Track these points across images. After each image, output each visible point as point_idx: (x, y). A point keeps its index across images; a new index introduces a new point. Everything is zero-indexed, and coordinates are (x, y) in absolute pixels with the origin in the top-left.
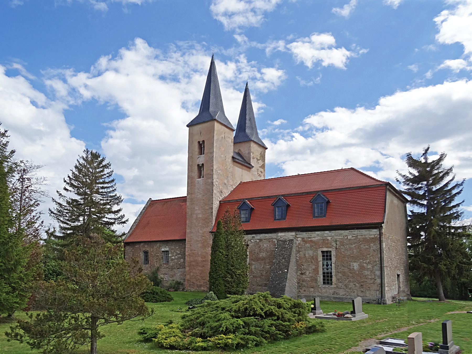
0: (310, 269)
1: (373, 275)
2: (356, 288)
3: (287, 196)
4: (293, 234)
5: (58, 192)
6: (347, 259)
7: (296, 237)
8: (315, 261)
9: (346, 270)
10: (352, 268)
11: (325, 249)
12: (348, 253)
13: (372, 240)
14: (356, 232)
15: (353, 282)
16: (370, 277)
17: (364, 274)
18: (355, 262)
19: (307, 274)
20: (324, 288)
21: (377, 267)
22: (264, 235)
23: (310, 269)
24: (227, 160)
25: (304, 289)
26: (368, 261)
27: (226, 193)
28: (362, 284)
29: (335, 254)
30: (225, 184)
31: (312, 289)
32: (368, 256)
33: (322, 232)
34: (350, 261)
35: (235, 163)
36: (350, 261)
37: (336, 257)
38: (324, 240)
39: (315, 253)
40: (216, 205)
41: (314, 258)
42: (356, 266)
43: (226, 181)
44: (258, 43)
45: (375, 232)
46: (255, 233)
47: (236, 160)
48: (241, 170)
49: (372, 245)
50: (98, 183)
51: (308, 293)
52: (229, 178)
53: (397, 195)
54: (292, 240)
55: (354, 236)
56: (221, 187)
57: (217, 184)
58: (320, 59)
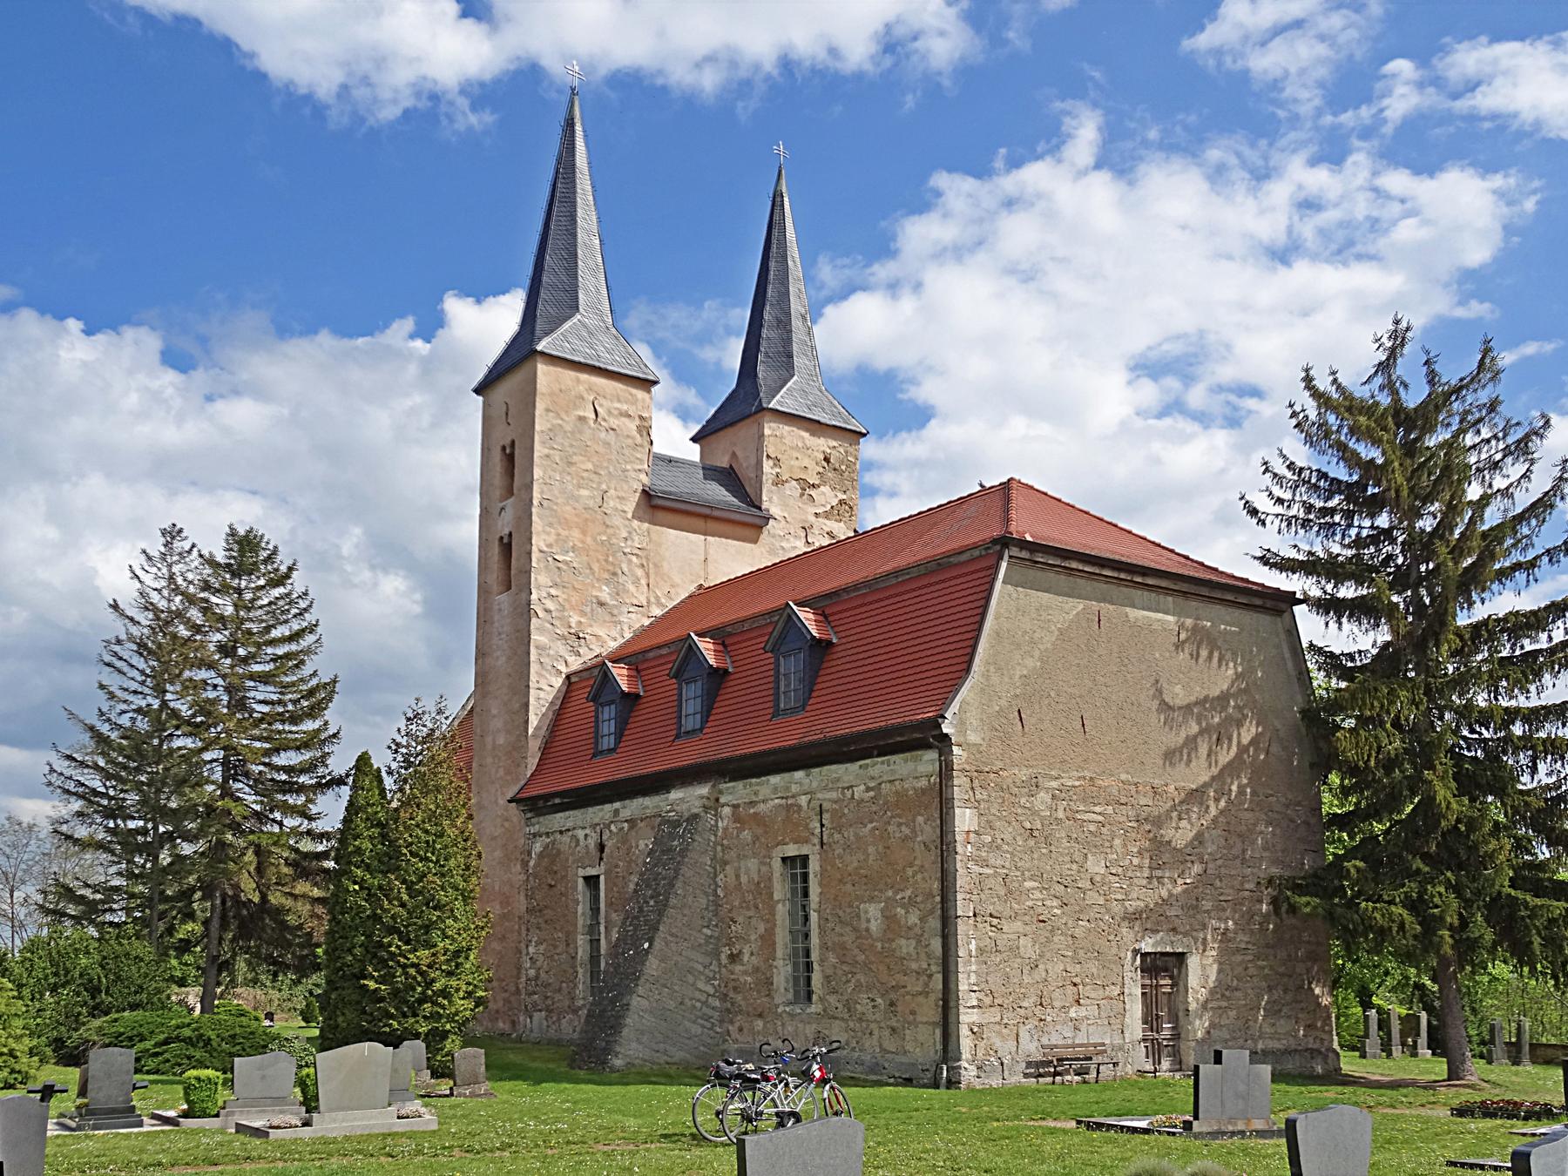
0: (753, 938)
1: (923, 956)
2: (878, 1016)
3: (730, 635)
4: (704, 790)
5: (102, 687)
6: (849, 887)
7: (714, 804)
8: (763, 902)
9: (849, 938)
10: (864, 925)
11: (792, 850)
12: (853, 862)
13: (904, 804)
14: (878, 767)
15: (869, 988)
16: (914, 966)
17: (898, 954)
18: (872, 899)
19: (746, 959)
20: (792, 1015)
21: (935, 923)
22: (641, 800)
23: (753, 938)
24: (611, 503)
25: (739, 1020)
26: (908, 893)
27: (607, 638)
28: (893, 996)
29: (818, 868)
30: (601, 604)
31: (759, 1024)
32: (910, 872)
33: (786, 776)
34: (857, 898)
35: (660, 515)
36: (857, 898)
37: (820, 884)
38: (788, 807)
39: (764, 869)
40: (544, 690)
41: (762, 888)
42: (873, 914)
43: (605, 593)
44: (1357, 107)
45: (928, 761)
46: (621, 798)
47: (660, 502)
48: (698, 539)
49: (920, 819)
50: (273, 642)
51: (750, 1039)
52: (622, 579)
53: (1150, 581)
54: (696, 816)
55: (872, 784)
56: (573, 621)
57: (550, 605)
58: (881, 28)
